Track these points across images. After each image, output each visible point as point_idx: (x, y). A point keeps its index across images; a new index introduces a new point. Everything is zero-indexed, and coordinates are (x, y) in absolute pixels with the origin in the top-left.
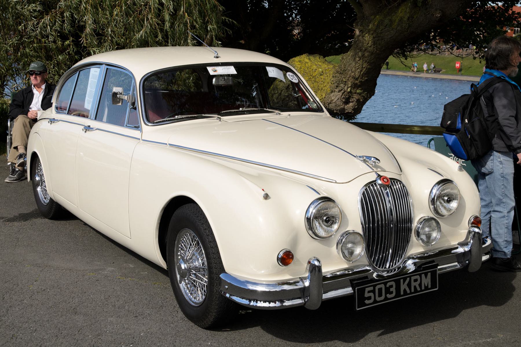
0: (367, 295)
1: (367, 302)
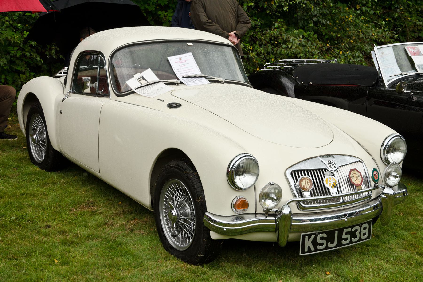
0: (344, 236)
1: (343, 242)
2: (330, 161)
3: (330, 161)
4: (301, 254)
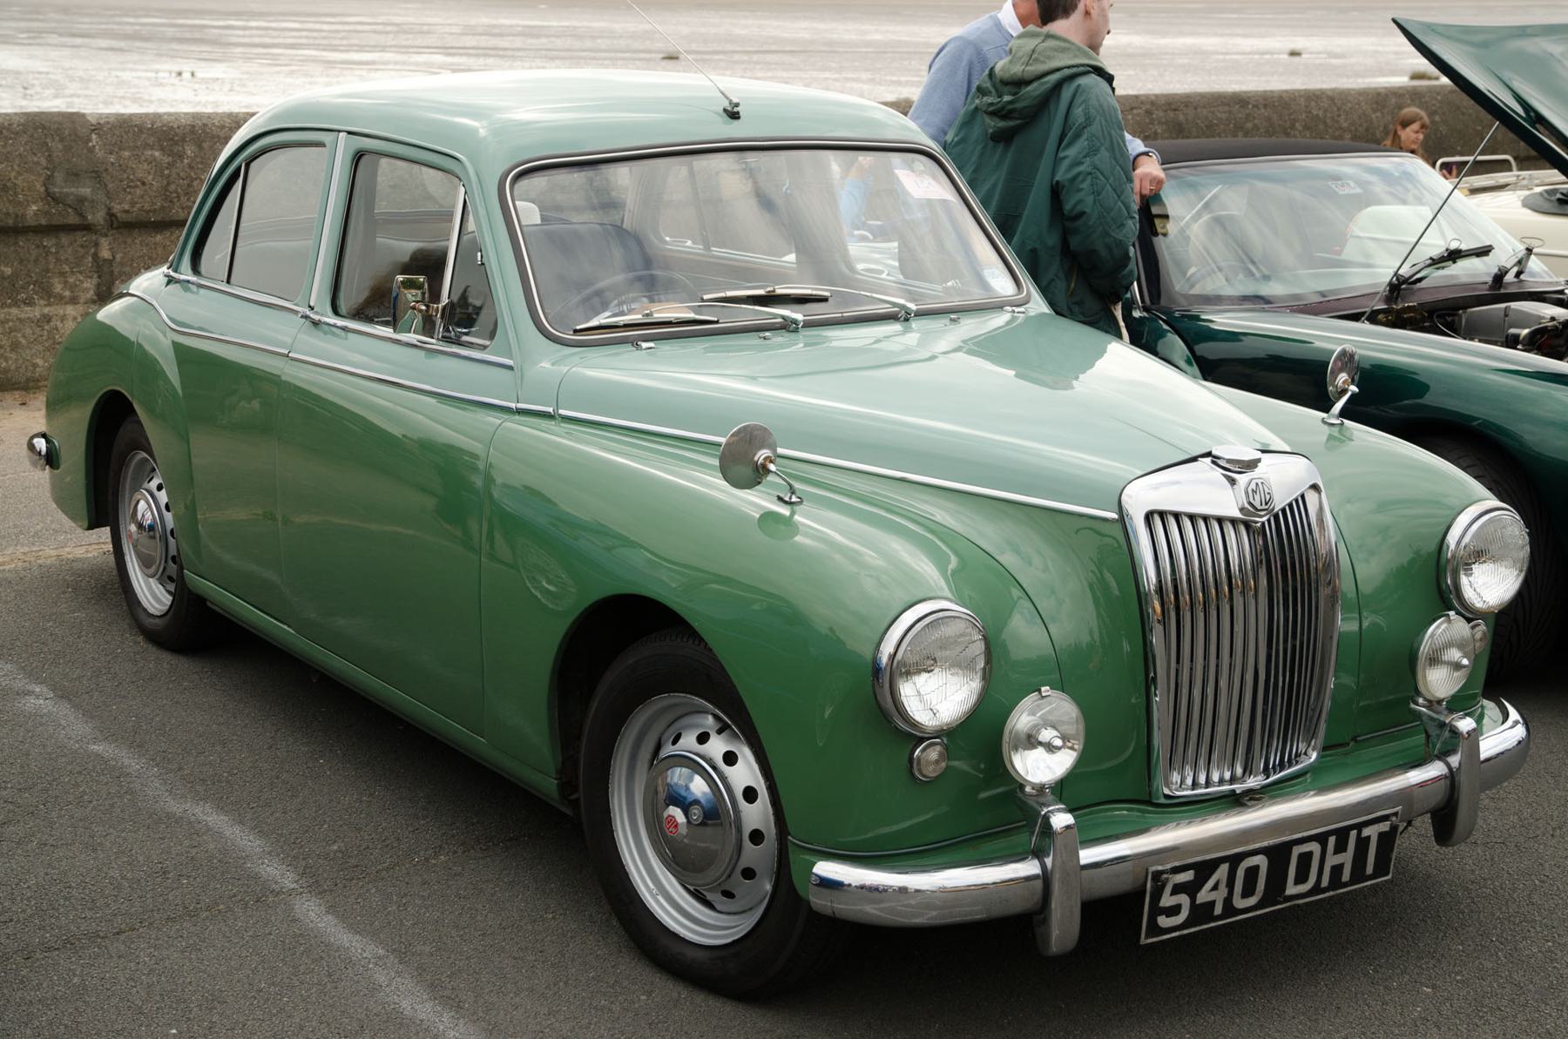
2: (1257, 484)
3: (1257, 484)
4: (1144, 941)
